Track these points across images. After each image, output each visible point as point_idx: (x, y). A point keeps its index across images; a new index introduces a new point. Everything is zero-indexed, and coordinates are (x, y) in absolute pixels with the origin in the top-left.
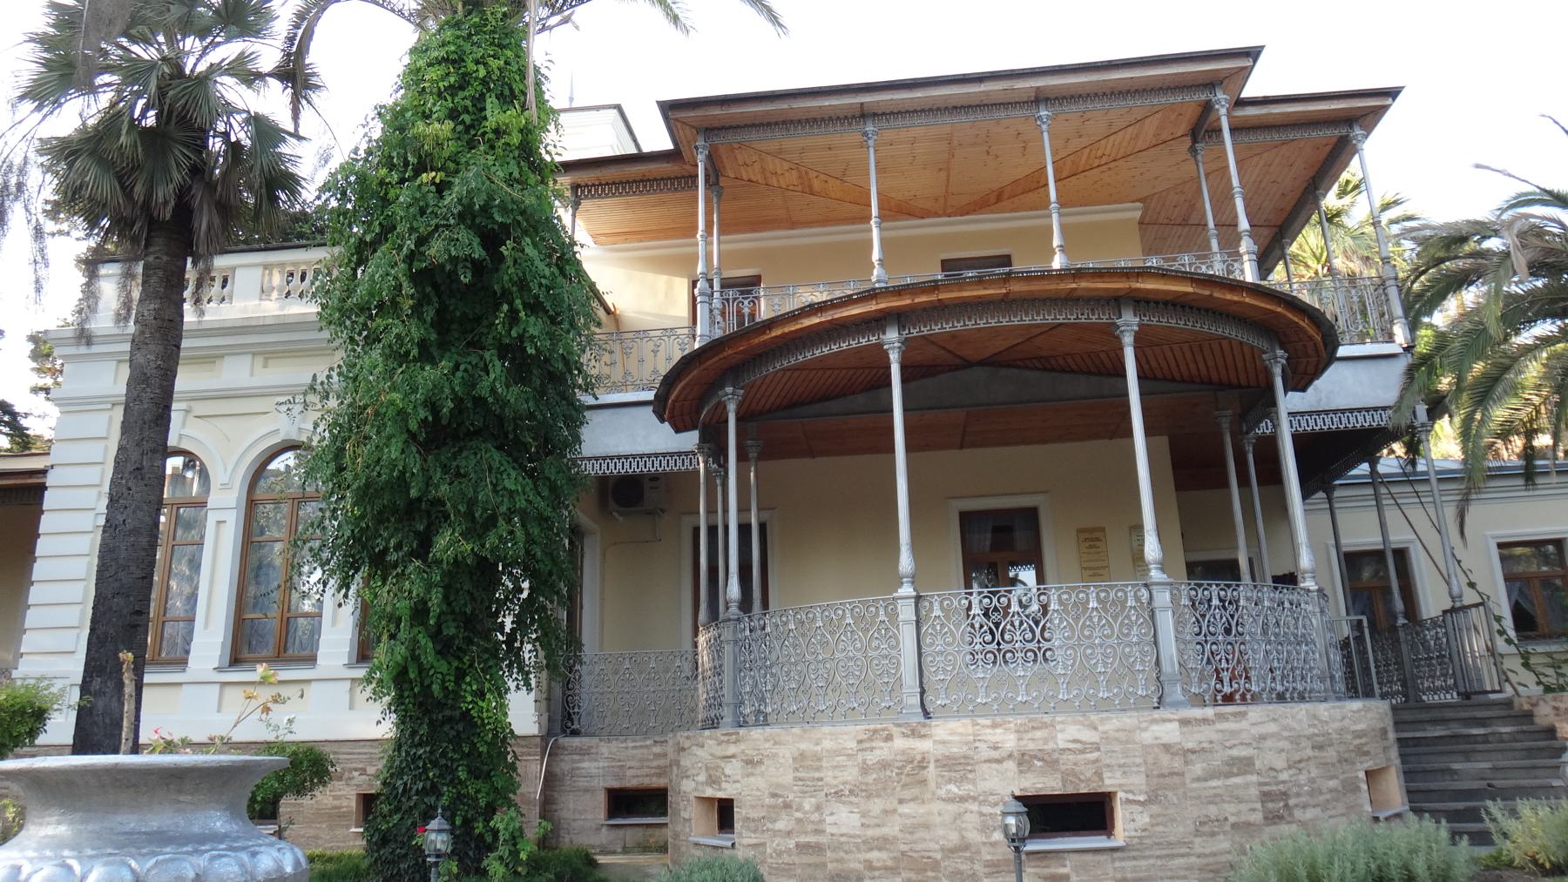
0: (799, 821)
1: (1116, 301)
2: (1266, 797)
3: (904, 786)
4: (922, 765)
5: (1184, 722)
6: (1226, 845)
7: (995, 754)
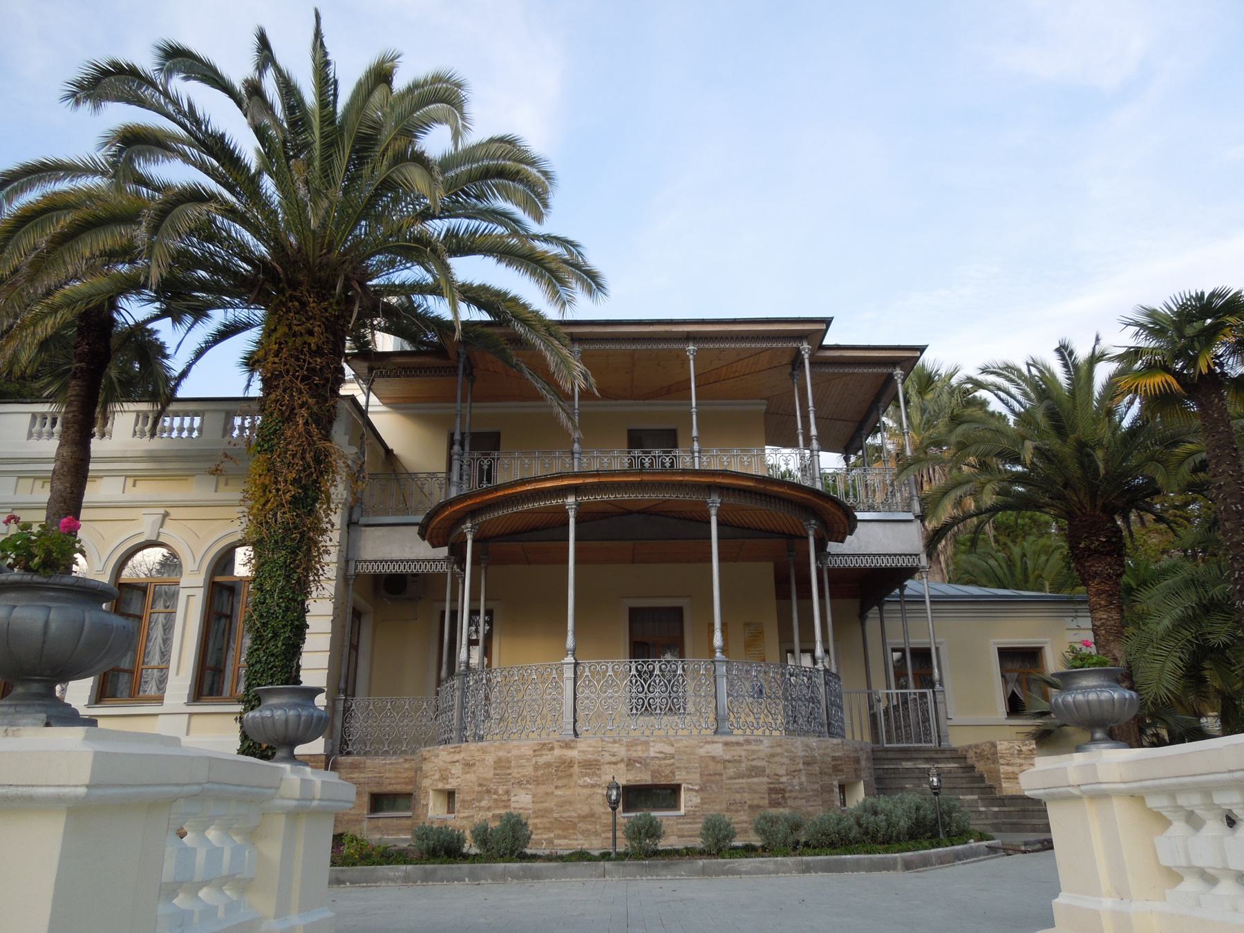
0: (496, 800)
1: (710, 488)
2: (771, 791)
3: (559, 778)
4: (570, 764)
5: (726, 744)
6: (745, 818)
7: (614, 759)
